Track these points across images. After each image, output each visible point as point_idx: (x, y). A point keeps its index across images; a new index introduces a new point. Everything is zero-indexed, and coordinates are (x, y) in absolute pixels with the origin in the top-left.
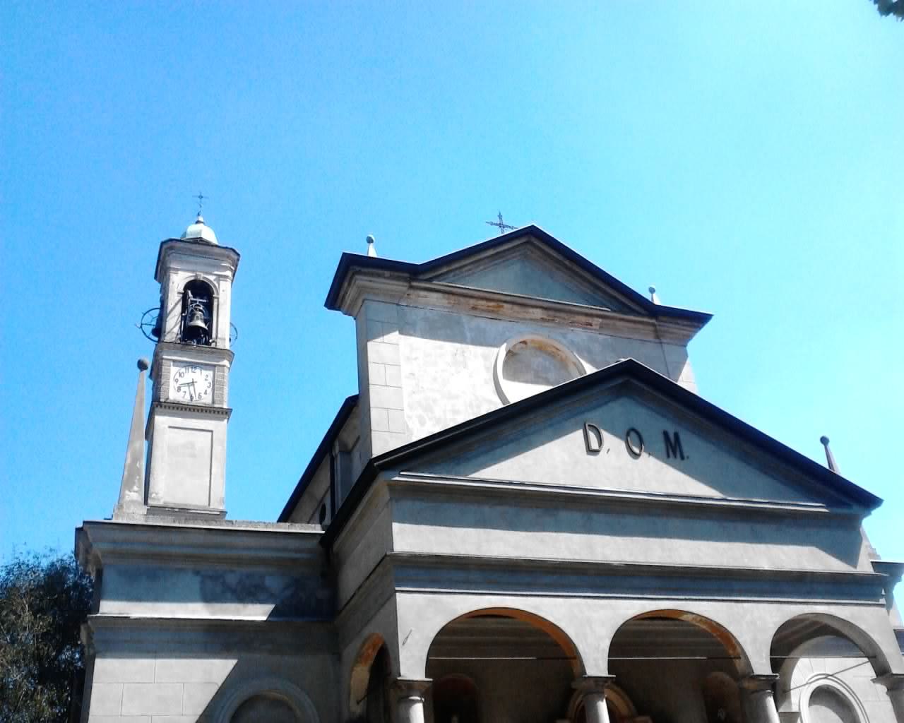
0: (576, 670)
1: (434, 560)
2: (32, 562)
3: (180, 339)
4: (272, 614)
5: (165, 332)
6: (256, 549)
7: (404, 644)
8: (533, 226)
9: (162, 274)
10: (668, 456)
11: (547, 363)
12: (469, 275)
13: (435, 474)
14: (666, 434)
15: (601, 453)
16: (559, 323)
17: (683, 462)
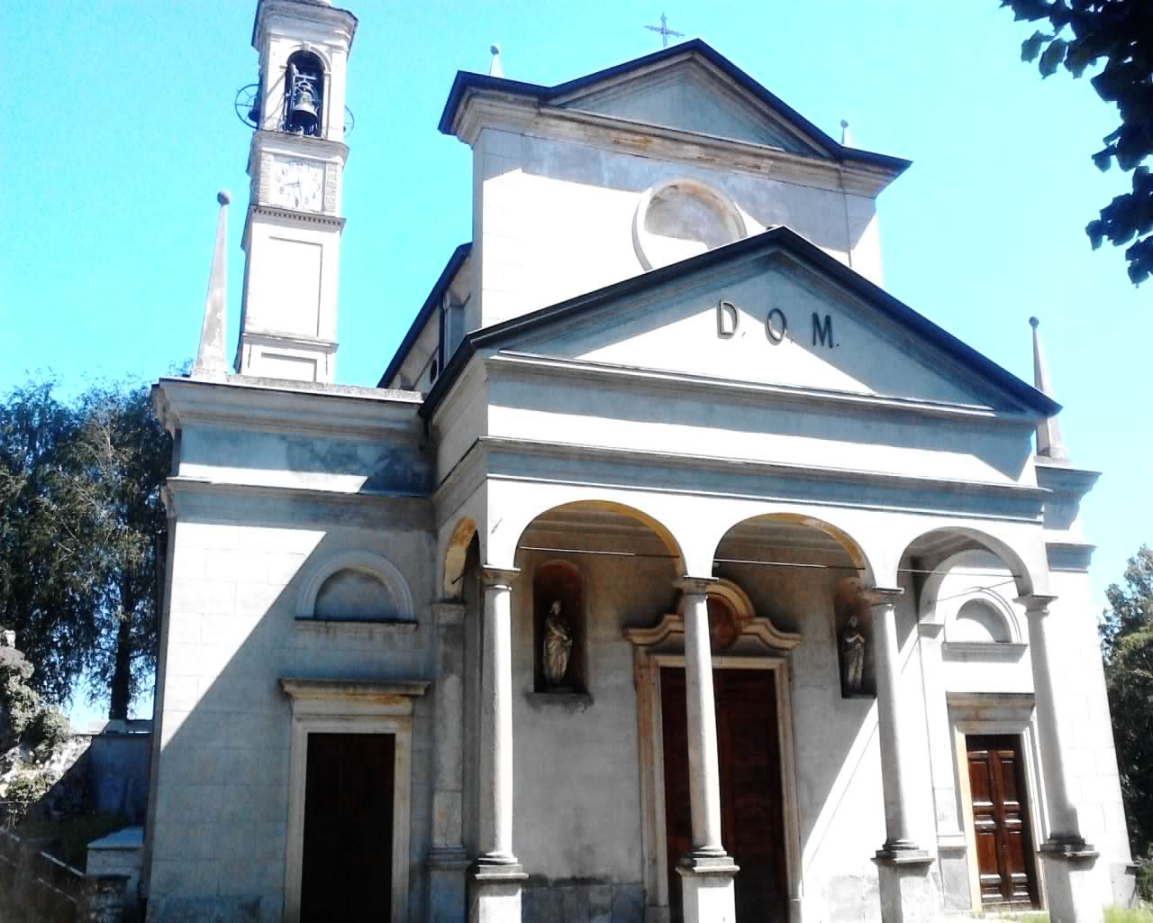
0: (679, 569)
1: (532, 447)
2: (111, 390)
3: (283, 126)
4: (364, 486)
5: (264, 116)
6: (350, 416)
7: (493, 532)
8: (698, 40)
9: (260, 39)
10: (814, 343)
11: (701, 215)
12: (613, 100)
13: (539, 353)
14: (815, 318)
15: (735, 336)
16: (720, 164)
17: (831, 350)
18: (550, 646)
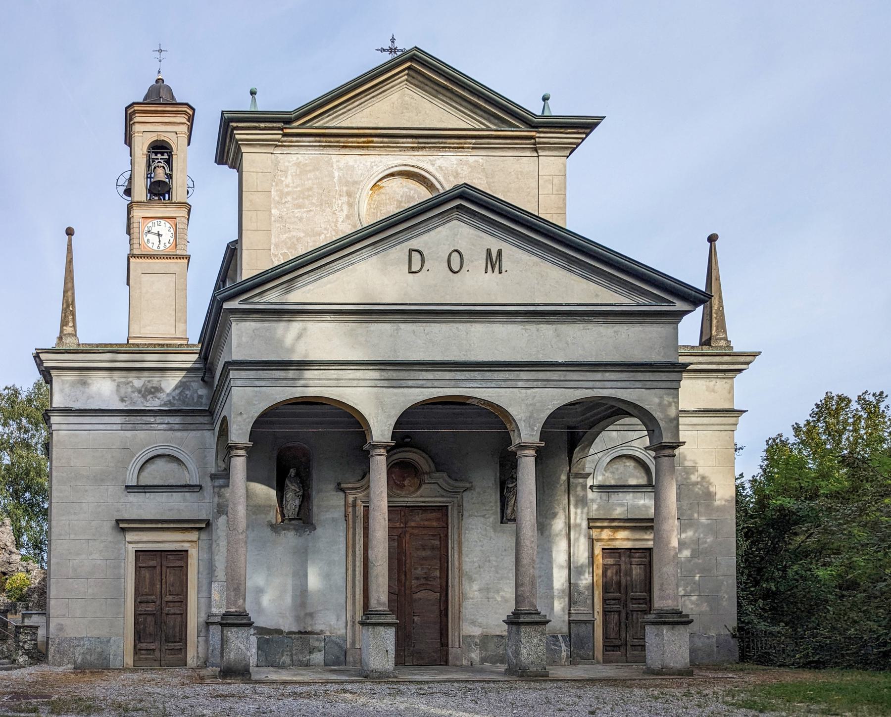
14: (489, 252)
18: (287, 496)
